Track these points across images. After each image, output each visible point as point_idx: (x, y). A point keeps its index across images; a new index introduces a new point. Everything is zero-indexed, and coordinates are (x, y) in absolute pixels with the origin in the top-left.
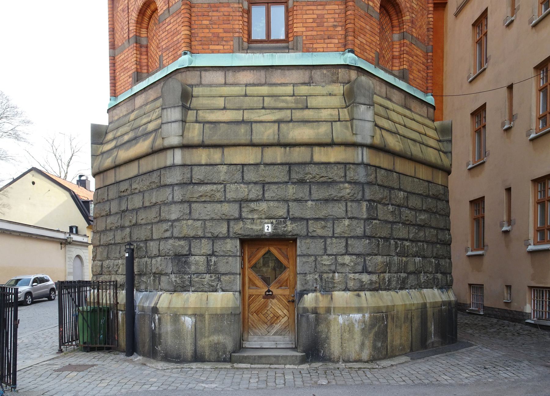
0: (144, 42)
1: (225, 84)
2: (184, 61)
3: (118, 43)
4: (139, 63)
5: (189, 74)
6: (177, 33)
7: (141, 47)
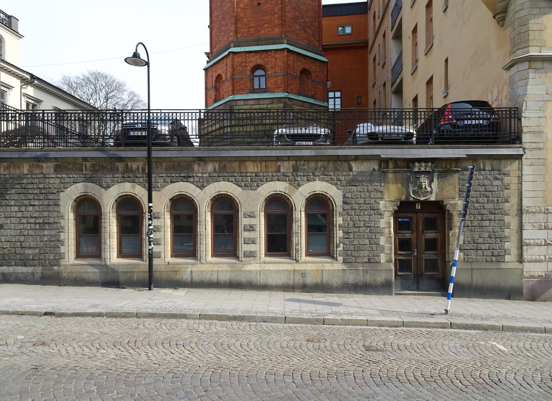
0: (218, 88)
1: (245, 105)
2: (231, 98)
3: (208, 87)
4: (216, 95)
5: (233, 102)
6: (229, 88)
7: (217, 89)
